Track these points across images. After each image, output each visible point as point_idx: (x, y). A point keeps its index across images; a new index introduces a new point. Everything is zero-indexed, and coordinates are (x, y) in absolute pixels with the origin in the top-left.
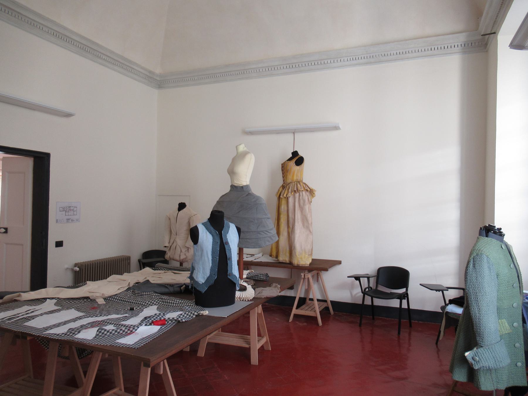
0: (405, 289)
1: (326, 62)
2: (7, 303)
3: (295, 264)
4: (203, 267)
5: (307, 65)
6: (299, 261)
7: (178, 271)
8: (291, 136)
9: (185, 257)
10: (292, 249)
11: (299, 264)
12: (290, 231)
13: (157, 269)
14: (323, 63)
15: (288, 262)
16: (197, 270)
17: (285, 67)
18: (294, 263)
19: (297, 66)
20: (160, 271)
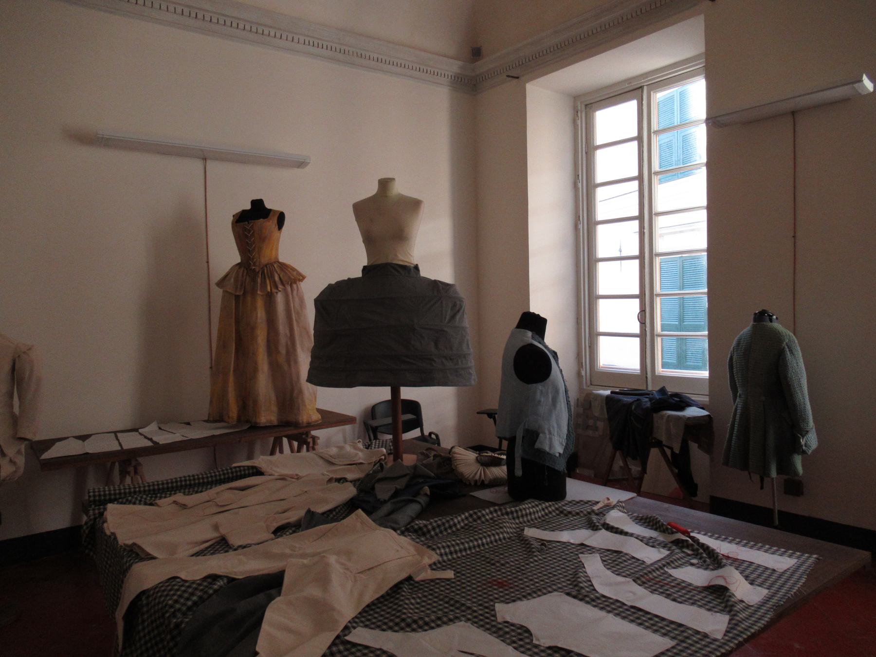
0: (419, 429)
1: (266, 32)
2: (807, 579)
3: (303, 422)
4: (558, 425)
5: (228, 23)
6: (310, 415)
7: (228, 482)
8: (196, 166)
9: (14, 469)
10: (295, 395)
11: (310, 420)
12: (282, 359)
13: (124, 500)
14: (260, 31)
15: (276, 423)
16: (547, 432)
17: (179, 10)
18: (301, 421)
19: (207, 18)
20: (199, 495)
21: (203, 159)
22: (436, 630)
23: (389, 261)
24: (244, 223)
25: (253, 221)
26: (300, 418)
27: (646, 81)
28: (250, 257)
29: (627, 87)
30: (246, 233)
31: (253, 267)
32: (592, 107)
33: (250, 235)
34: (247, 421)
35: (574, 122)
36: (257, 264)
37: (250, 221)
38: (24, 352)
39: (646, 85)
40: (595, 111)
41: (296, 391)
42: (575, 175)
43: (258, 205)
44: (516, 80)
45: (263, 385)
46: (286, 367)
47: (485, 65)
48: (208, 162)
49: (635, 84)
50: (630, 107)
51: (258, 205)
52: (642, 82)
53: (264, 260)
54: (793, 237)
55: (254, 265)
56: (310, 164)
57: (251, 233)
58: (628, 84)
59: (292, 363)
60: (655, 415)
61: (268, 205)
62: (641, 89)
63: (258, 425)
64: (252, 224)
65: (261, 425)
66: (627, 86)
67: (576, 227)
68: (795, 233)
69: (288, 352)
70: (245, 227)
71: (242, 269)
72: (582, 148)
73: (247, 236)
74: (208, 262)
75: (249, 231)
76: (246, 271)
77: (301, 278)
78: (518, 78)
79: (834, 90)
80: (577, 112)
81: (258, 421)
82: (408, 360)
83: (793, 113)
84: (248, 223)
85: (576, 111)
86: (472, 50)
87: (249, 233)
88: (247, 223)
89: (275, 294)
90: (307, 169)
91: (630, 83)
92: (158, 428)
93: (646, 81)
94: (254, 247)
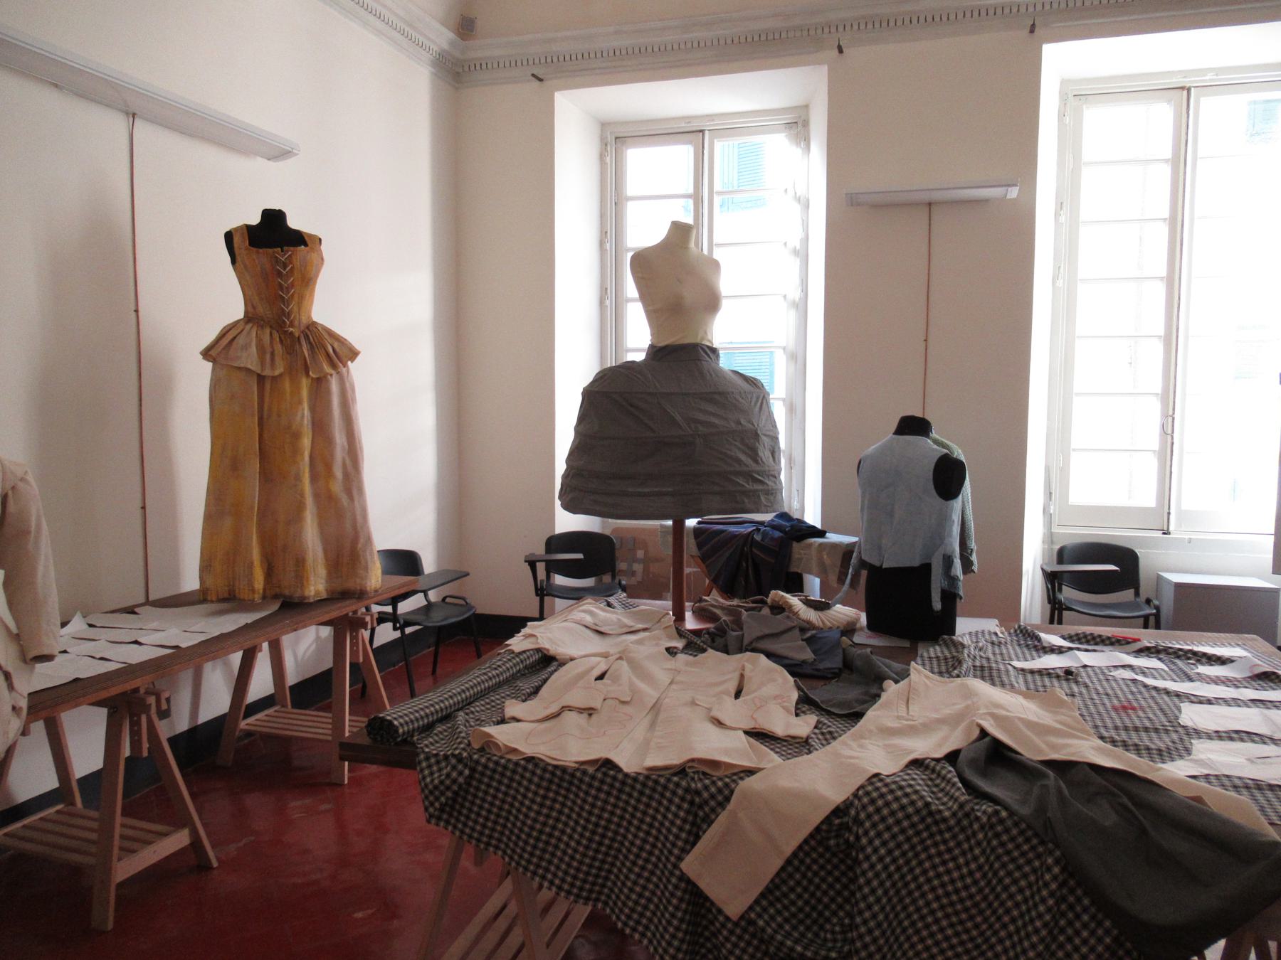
12: (337, 487)
15: (324, 596)
21: (127, 114)
22: (1213, 742)
23: (698, 341)
24: (275, 250)
25: (292, 248)
26: (369, 584)
27: (711, 125)
28: (283, 310)
29: (684, 126)
30: (278, 267)
31: (291, 329)
32: (625, 142)
33: (285, 272)
34: (276, 597)
35: (602, 158)
36: (296, 323)
37: (285, 248)
38: (22, 480)
39: (709, 130)
40: (627, 149)
41: (362, 541)
42: (601, 232)
43: (273, 218)
44: (538, 83)
45: (311, 537)
46: (345, 500)
47: (481, 49)
48: (138, 122)
49: (696, 125)
50: (682, 154)
51: (273, 218)
52: (706, 125)
53: (304, 321)
54: (135, 311)
55: (292, 325)
56: (298, 156)
57: (288, 269)
58: (685, 123)
59: (355, 493)
60: (795, 544)
61: (293, 222)
62: (701, 133)
63: (306, 601)
64: (290, 253)
65: (312, 600)
66: (684, 125)
67: (602, 302)
68: (927, 337)
69: (346, 476)
70: (276, 257)
71: (268, 331)
72: (611, 196)
73: (279, 274)
74: (137, 311)
75: (285, 267)
76: (276, 335)
77: (354, 354)
78: (541, 80)
79: (974, 190)
80: (606, 145)
81: (307, 593)
82: (760, 478)
83: (930, 204)
84: (282, 251)
85: (604, 144)
86: (463, 20)
87: (285, 269)
88: (280, 249)
89: (329, 377)
90: (289, 163)
91: (689, 122)
92: (87, 626)
93: (711, 125)
94: (293, 295)
